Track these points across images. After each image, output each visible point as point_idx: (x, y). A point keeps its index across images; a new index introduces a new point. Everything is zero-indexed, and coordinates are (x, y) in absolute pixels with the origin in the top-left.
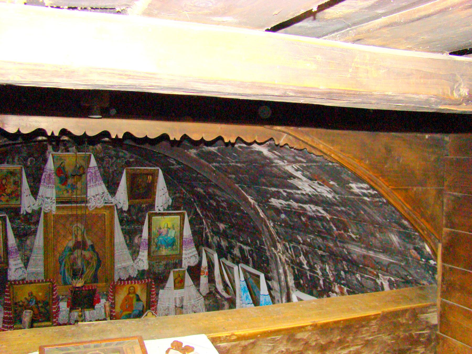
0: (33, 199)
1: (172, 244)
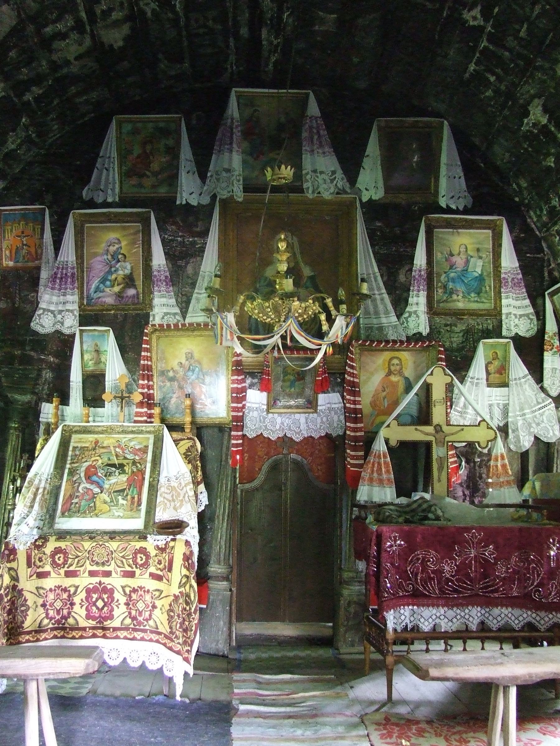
0: (198, 181)
1: (478, 286)
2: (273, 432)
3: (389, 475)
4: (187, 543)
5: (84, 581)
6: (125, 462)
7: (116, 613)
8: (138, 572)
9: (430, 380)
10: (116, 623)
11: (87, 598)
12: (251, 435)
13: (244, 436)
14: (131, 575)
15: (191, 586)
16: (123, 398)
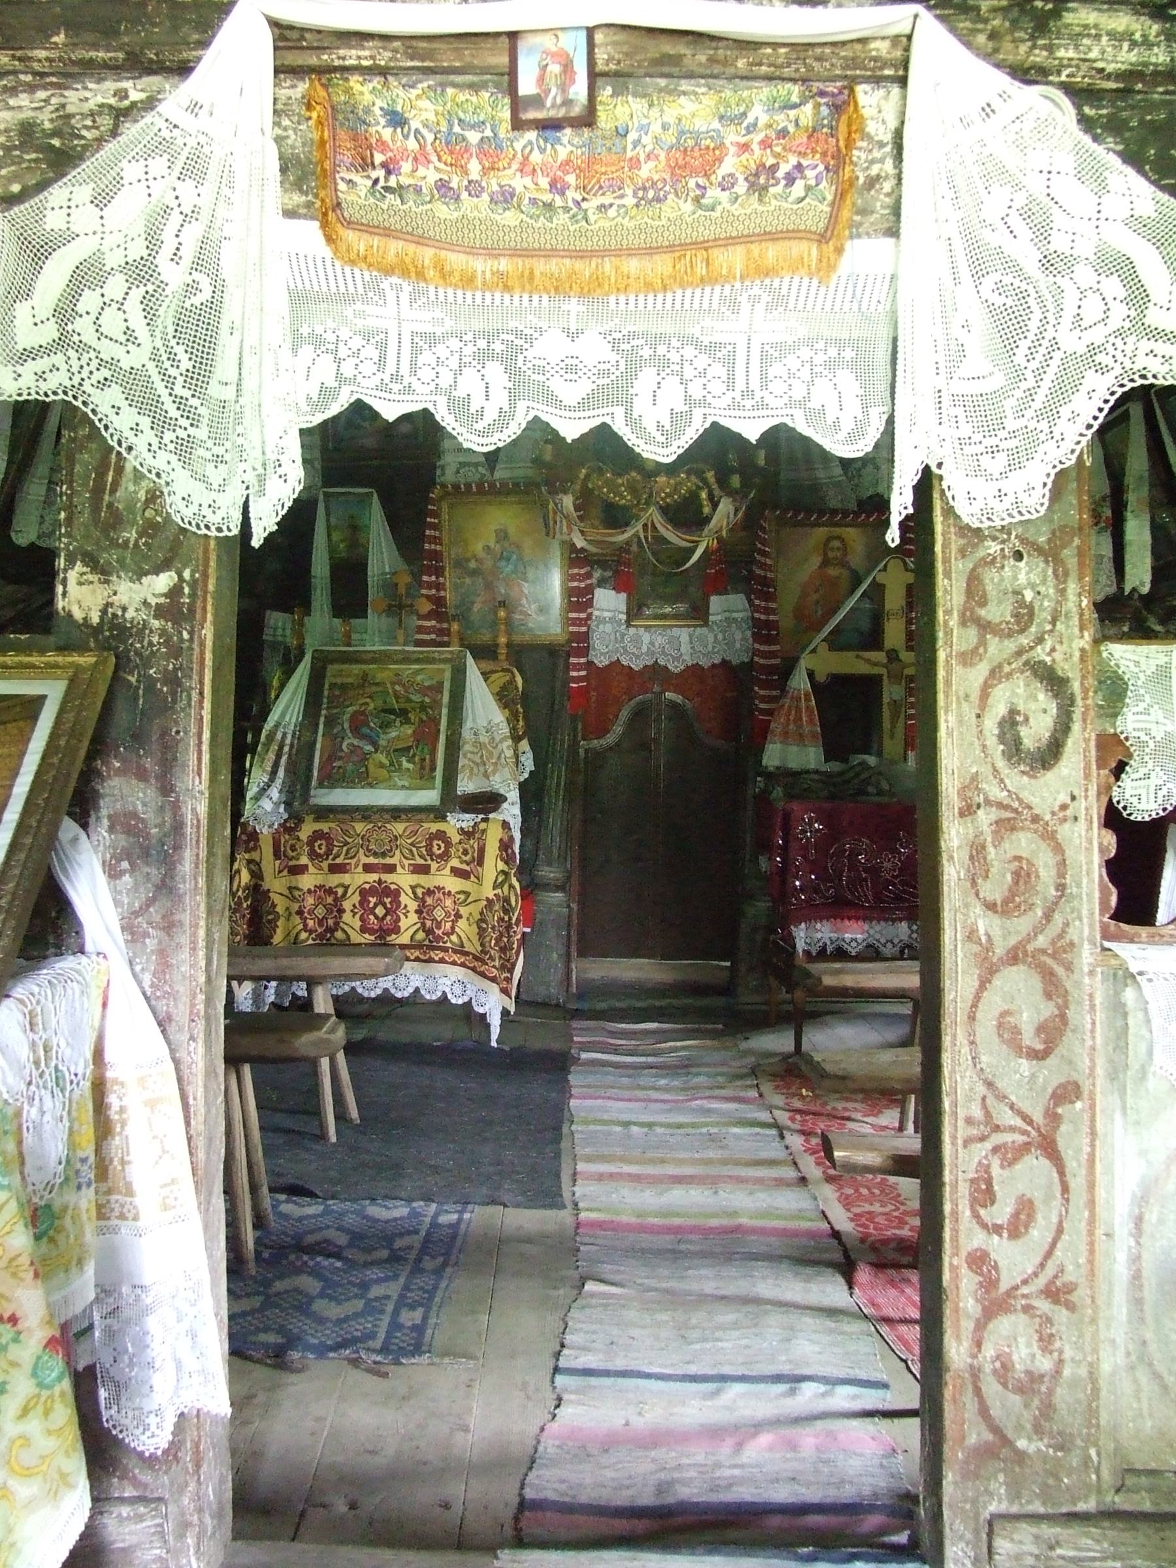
2: (637, 657)
3: (811, 725)
4: (505, 825)
5: (358, 879)
6: (408, 706)
7: (404, 923)
8: (434, 866)
9: (881, 578)
10: (405, 939)
11: (361, 903)
12: (601, 661)
13: (590, 664)
14: (423, 870)
15: (511, 886)
16: (397, 607)
